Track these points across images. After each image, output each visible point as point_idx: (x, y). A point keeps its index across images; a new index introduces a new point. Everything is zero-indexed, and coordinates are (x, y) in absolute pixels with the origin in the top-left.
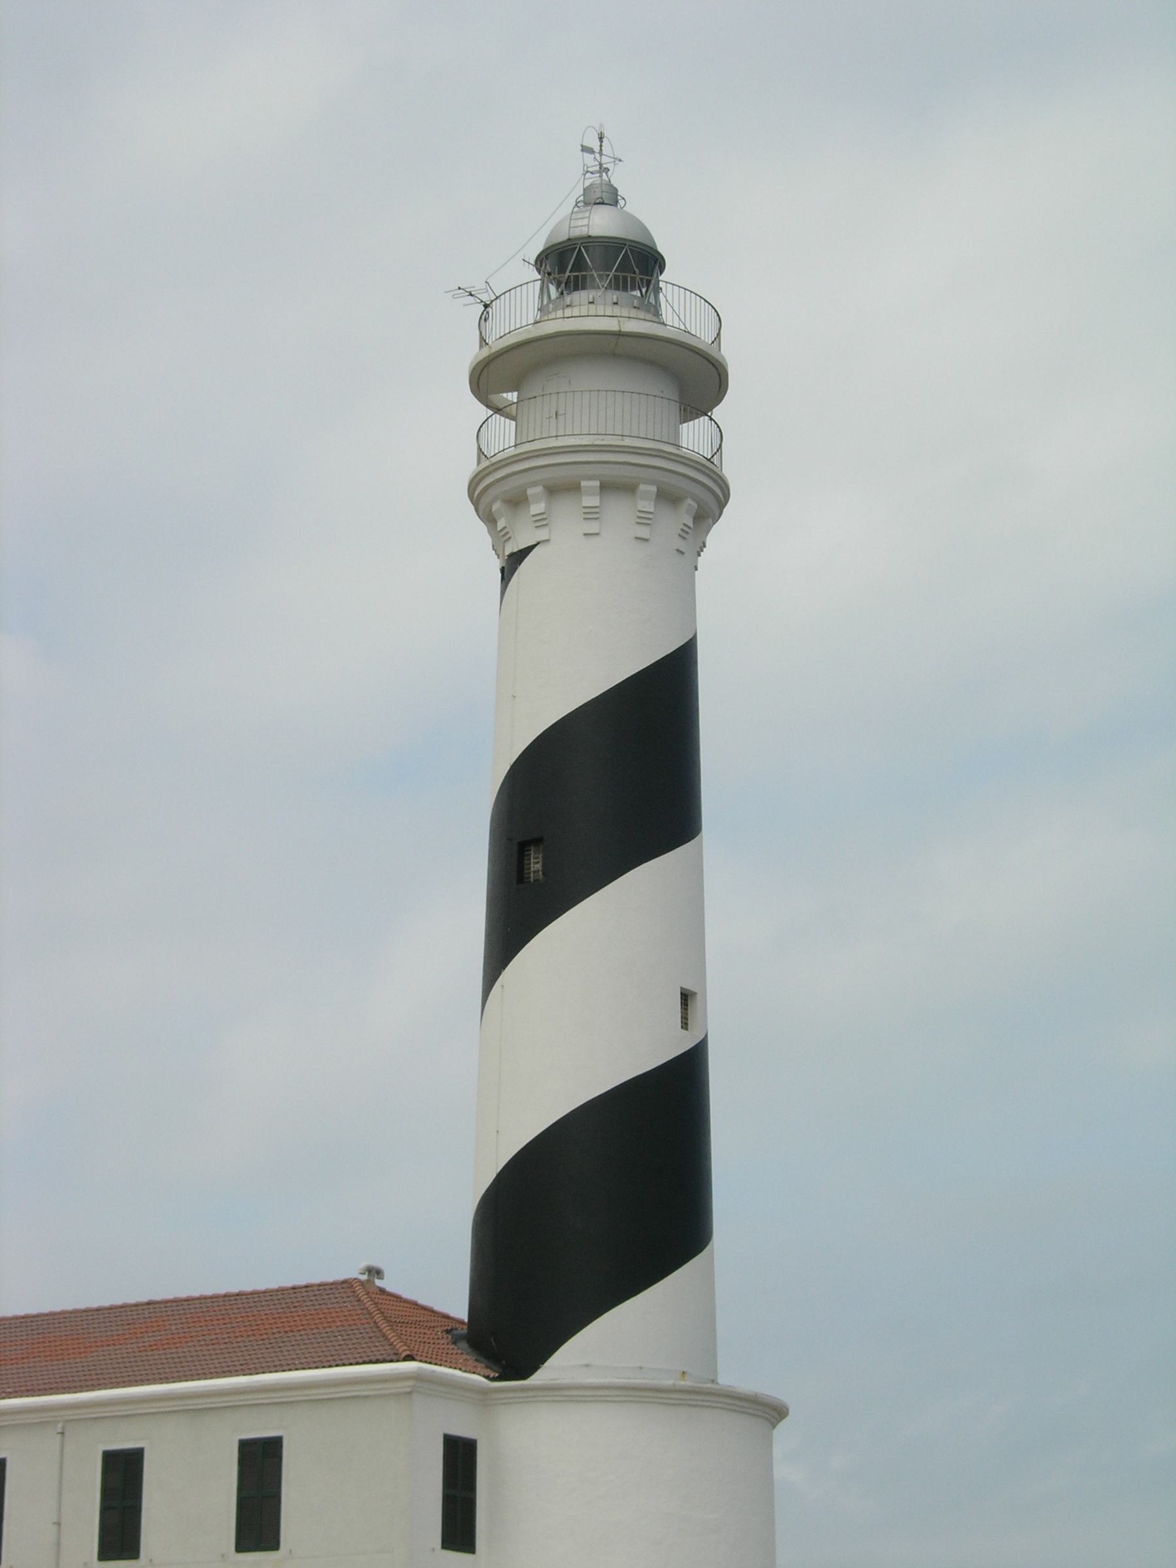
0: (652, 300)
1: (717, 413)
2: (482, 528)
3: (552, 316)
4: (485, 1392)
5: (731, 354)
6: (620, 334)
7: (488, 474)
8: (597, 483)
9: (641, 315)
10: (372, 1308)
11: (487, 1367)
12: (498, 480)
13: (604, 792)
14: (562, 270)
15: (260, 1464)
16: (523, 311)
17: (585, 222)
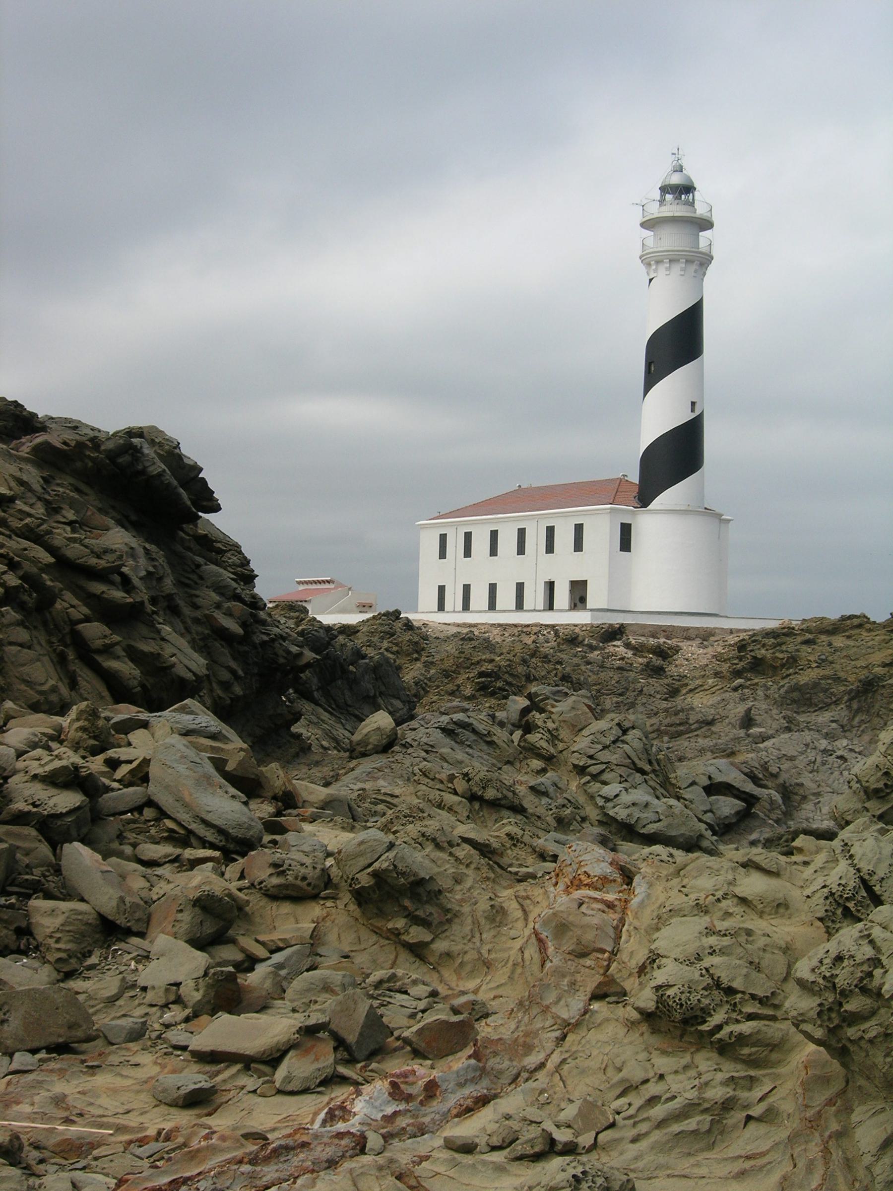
11: (117, 671)
15: (579, 529)
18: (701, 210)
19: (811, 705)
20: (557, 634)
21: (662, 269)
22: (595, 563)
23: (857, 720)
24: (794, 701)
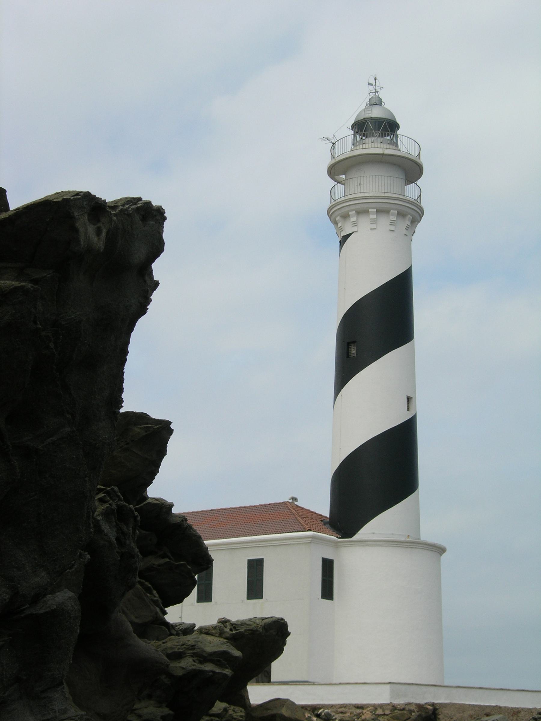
0: (395, 140)
1: (419, 182)
2: (332, 226)
3: (358, 147)
4: (336, 542)
5: (424, 161)
6: (383, 155)
7: (332, 209)
8: (375, 210)
9: (391, 147)
10: (294, 512)
12: (339, 209)
13: (378, 324)
14: (362, 131)
15: (255, 568)
16: (347, 147)
17: (370, 112)
19: (394, 706)
21: (364, 224)
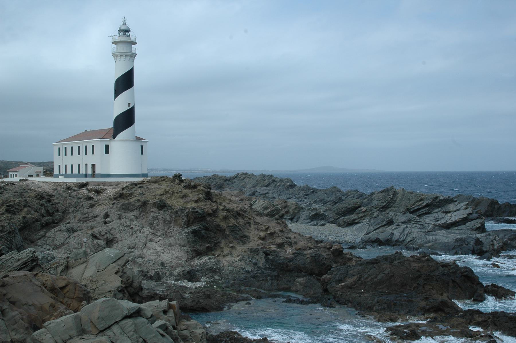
18: (132, 39)
19: (129, 210)
20: (66, 185)
22: (97, 158)
23: (141, 215)
24: (123, 209)
